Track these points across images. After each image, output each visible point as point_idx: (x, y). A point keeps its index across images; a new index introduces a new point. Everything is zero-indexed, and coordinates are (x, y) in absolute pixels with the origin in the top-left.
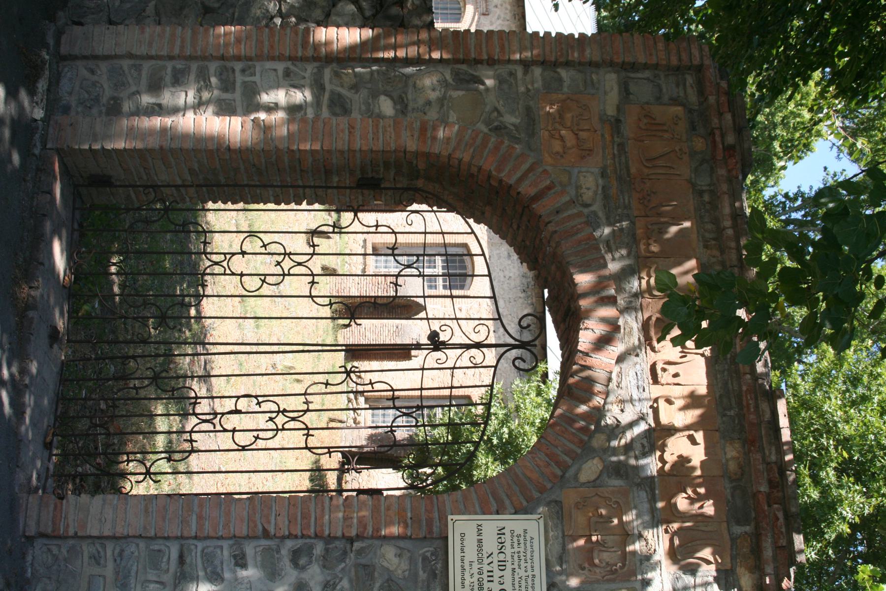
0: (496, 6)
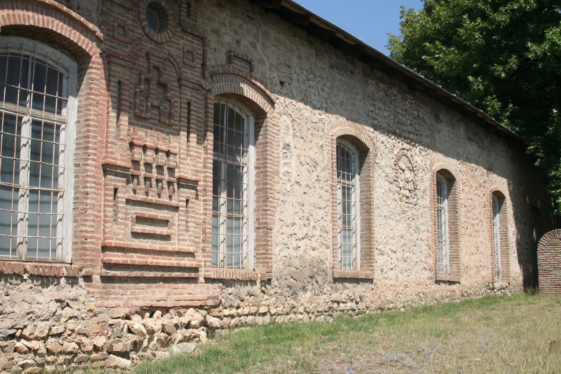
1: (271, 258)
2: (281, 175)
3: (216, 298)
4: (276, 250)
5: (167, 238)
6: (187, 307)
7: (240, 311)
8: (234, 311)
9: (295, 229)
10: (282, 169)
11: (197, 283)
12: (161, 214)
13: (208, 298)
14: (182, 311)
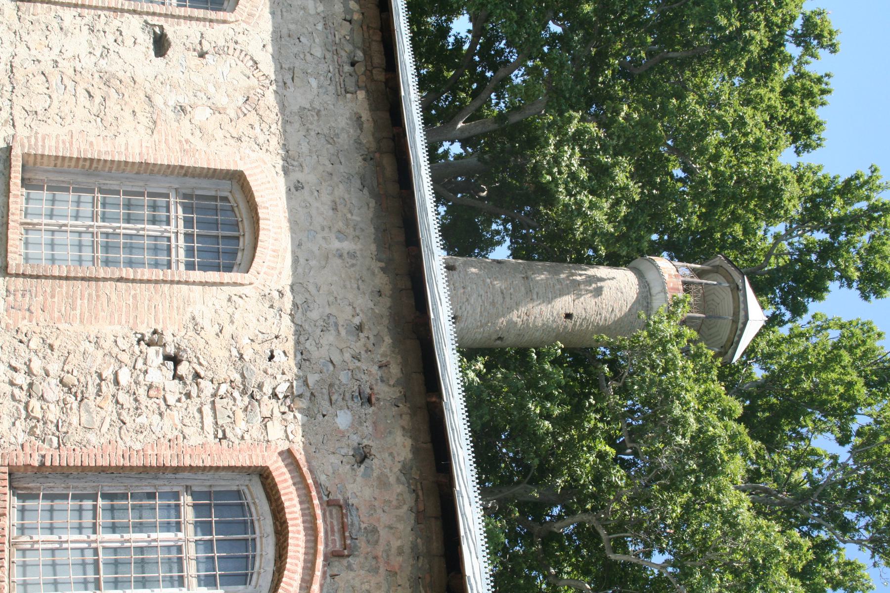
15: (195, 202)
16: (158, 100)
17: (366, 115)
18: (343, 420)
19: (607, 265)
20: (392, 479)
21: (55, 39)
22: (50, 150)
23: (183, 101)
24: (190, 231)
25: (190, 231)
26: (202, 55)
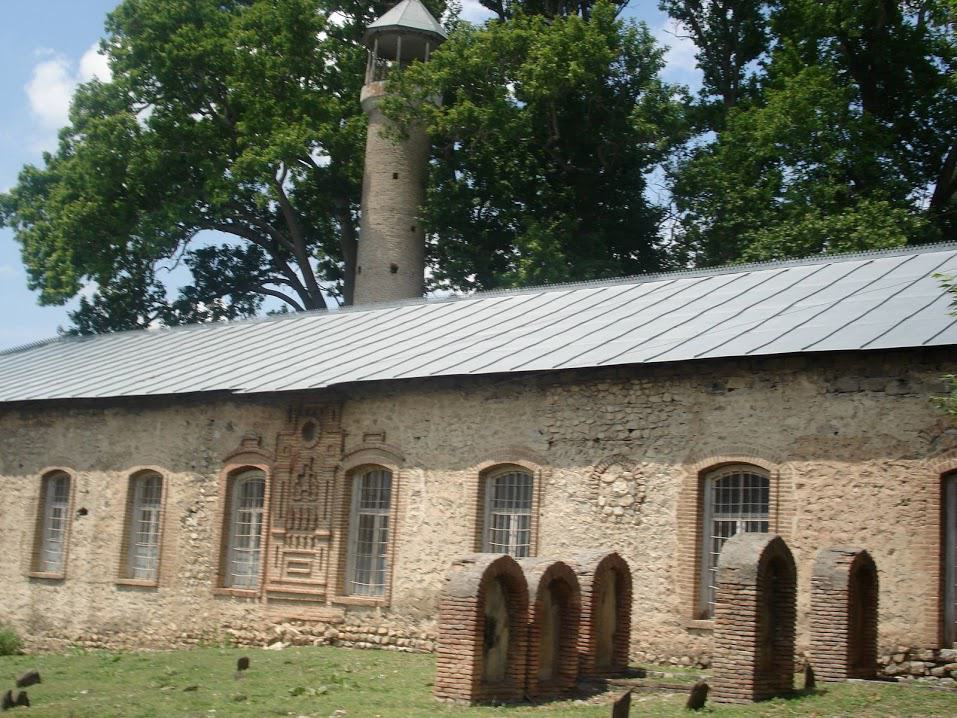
0: (375, 421)
1: (927, 625)
2: (408, 520)
3: (339, 617)
4: (397, 583)
5: (308, 575)
6: (318, 621)
7: (361, 629)
8: (355, 629)
9: (421, 564)
10: (409, 514)
11: (324, 606)
12: (307, 560)
13: (334, 617)
14: (314, 623)
15: (515, 500)
16: (103, 514)
17: (114, 411)
18: (217, 435)
19: (701, 264)
20: (239, 413)
21: (78, 563)
22: (117, 566)
23: (103, 502)
24: (730, 508)
25: (506, 504)
26: (87, 492)
